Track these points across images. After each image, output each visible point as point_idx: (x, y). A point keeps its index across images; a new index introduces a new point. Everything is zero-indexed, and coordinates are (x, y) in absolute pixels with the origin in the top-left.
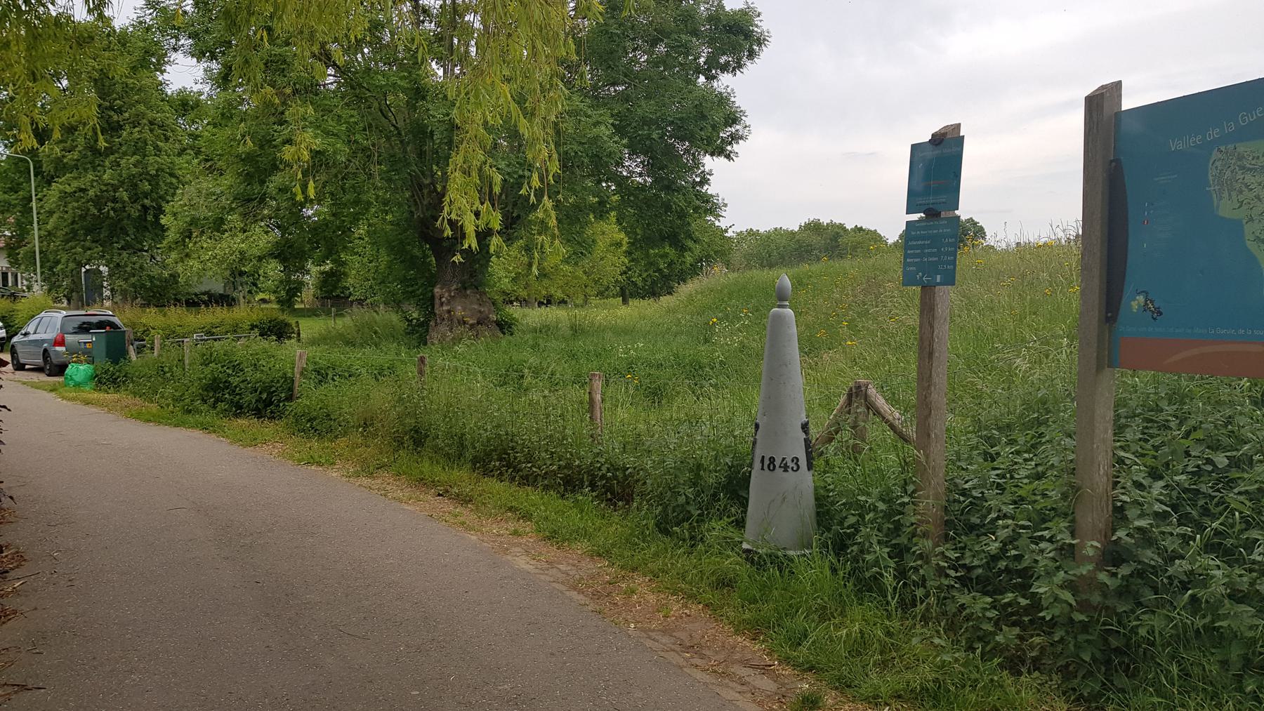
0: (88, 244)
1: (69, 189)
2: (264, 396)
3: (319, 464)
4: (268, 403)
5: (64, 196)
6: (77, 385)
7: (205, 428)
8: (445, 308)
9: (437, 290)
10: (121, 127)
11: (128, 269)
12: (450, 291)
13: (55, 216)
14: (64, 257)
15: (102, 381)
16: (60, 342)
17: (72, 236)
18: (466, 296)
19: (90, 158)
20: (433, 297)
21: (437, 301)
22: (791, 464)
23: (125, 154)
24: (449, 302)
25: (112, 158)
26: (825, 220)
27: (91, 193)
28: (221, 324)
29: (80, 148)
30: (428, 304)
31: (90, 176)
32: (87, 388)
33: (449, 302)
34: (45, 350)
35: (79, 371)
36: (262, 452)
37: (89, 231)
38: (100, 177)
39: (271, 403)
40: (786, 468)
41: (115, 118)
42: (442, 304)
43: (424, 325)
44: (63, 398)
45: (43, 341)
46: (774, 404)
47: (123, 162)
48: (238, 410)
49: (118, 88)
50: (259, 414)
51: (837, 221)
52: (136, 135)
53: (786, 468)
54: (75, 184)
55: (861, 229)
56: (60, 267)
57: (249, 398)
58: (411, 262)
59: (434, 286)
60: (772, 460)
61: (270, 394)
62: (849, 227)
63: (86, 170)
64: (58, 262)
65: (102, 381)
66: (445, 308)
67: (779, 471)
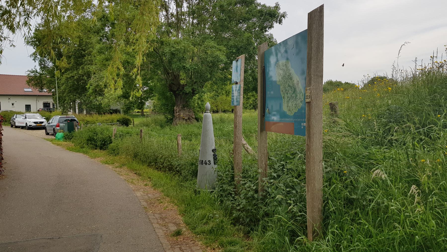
0: (75, 94)
1: (68, 76)
2: (103, 143)
3: (108, 164)
4: (104, 145)
5: (67, 79)
6: (59, 139)
7: (84, 152)
8: (178, 114)
9: (175, 108)
10: (85, 56)
11: (87, 102)
12: (179, 108)
13: (64, 85)
14: (67, 98)
15: (66, 138)
16: (58, 126)
17: (70, 92)
18: (184, 110)
19: (75, 67)
20: (174, 110)
21: (175, 112)
22: (208, 162)
23: (86, 64)
24: (179, 112)
25: (82, 66)
26: (334, 80)
27: (75, 77)
28: (109, 120)
29: (72, 63)
30: (172, 112)
31: (75, 72)
32: (62, 140)
33: (179, 112)
34: (54, 129)
35: (60, 135)
36: (97, 160)
37: (75, 90)
38: (78, 72)
39: (105, 145)
40: (206, 164)
41: (83, 53)
42: (176, 113)
43: (172, 120)
44: (53, 143)
45: (53, 126)
46: (204, 145)
47: (85, 67)
48: (96, 147)
49: (84, 43)
50: (101, 148)
51: (338, 80)
52: (89, 58)
53: (206, 164)
54: (71, 75)
55: (347, 83)
56: (66, 101)
57: (99, 143)
58: (166, 98)
59: (174, 106)
60: (202, 161)
61: (105, 142)
62: (343, 82)
63: (74, 70)
64: (65, 100)
65: (66, 138)
66: (178, 114)
67: (204, 164)
